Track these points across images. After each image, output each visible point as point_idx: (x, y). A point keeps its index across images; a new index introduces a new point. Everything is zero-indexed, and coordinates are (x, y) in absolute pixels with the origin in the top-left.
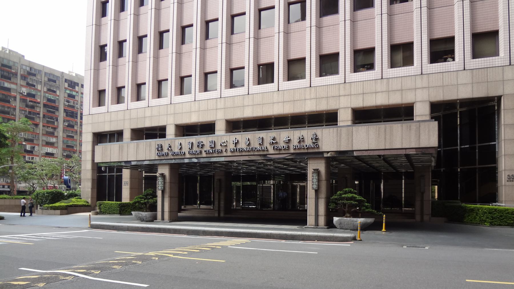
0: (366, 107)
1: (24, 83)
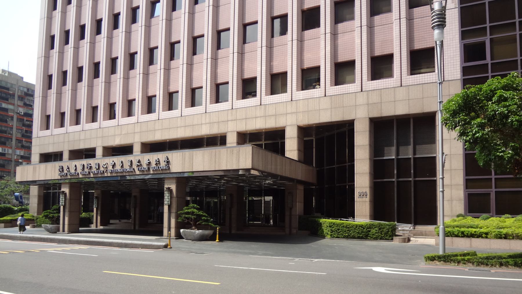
1: (21, 103)
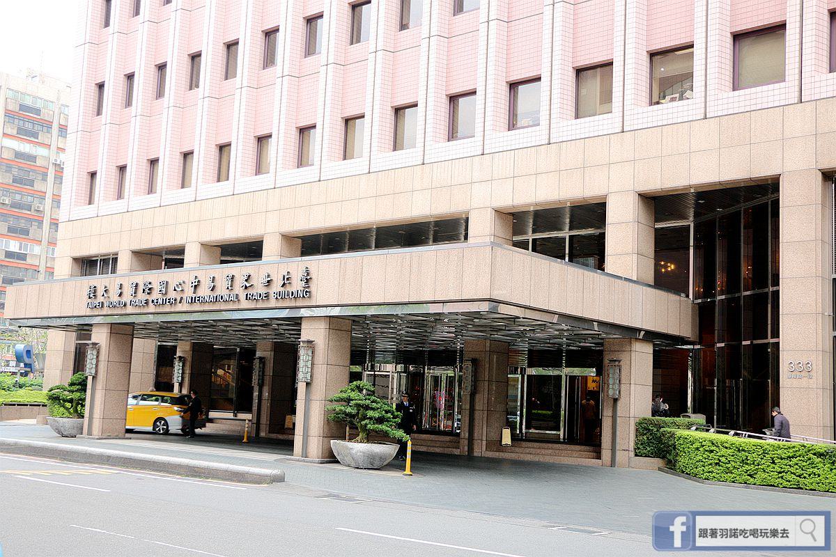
0: (518, 206)
